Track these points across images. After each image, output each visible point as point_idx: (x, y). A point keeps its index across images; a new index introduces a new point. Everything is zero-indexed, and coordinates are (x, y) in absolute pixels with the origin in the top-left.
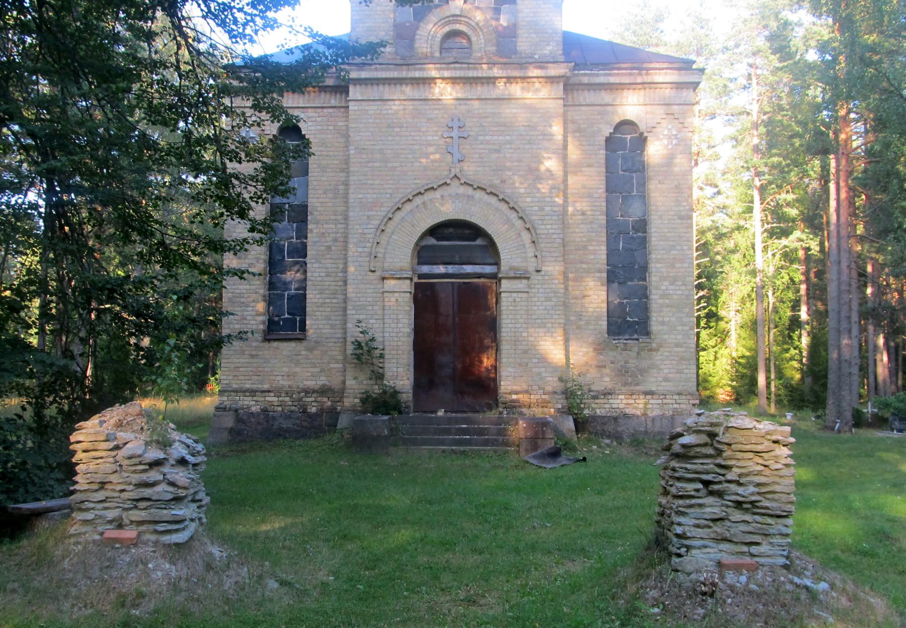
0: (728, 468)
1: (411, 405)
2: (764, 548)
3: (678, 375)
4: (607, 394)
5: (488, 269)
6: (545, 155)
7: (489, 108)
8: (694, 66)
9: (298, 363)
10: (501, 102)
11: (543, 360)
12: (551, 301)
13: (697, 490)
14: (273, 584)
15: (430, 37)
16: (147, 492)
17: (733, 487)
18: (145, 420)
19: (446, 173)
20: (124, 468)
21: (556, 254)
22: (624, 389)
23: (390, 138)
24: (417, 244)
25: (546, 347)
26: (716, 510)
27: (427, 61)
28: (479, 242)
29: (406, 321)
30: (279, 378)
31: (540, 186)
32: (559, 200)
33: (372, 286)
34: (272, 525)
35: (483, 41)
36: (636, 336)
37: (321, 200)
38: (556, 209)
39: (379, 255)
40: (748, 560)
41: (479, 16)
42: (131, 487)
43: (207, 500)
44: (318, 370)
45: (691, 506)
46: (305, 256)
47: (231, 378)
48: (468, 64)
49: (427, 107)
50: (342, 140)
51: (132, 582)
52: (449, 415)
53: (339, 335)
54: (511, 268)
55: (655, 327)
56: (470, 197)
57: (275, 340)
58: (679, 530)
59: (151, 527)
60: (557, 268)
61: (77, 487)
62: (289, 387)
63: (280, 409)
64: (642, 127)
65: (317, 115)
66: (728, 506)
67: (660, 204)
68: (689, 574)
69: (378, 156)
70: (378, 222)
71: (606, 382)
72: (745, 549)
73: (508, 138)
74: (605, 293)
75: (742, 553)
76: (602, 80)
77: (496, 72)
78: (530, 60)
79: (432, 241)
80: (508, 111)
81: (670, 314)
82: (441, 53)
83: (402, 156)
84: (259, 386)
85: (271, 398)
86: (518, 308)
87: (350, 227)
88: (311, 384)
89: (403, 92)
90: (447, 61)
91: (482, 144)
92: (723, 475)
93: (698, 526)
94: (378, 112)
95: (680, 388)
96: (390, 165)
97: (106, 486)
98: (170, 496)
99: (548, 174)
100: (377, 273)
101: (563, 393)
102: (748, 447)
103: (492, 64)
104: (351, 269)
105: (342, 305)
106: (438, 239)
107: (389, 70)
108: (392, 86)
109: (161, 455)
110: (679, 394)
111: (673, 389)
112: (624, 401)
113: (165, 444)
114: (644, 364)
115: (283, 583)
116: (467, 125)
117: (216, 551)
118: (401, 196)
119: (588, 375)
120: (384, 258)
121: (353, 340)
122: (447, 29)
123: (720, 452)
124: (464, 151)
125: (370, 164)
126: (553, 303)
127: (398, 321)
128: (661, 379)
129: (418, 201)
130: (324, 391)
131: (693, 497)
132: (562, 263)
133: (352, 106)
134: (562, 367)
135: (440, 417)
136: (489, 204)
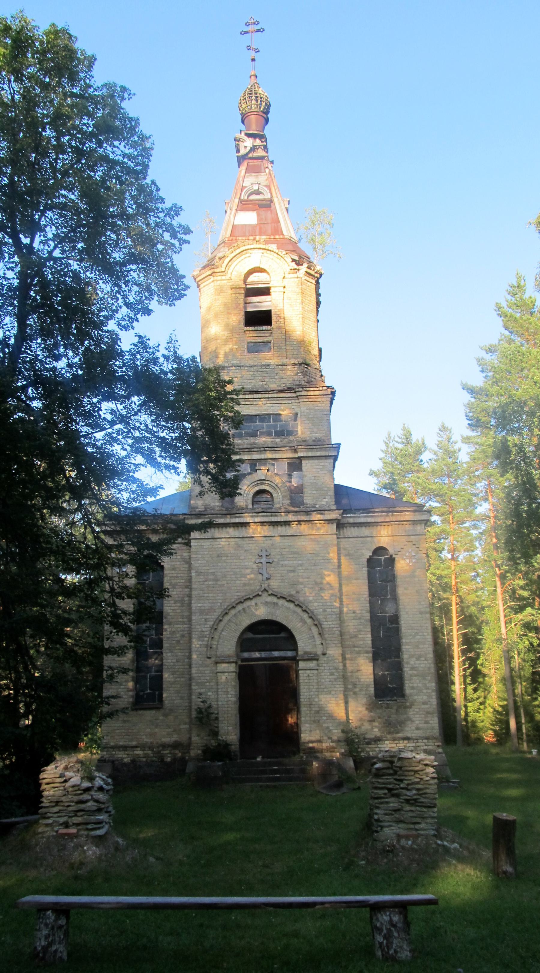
0: (401, 781)
1: (238, 754)
2: (423, 826)
3: (426, 725)
4: (377, 740)
5: (290, 654)
6: (326, 573)
7: (287, 542)
8: (425, 509)
9: (157, 726)
10: (294, 538)
11: (331, 717)
13: (385, 794)
14: (152, 859)
16: (82, 806)
17: (404, 791)
18: (80, 765)
19: (258, 588)
20: (70, 793)
21: (336, 642)
22: (389, 736)
23: (220, 564)
24: (240, 637)
25: (332, 708)
26: (395, 805)
27: (244, 511)
28: (283, 635)
29: (234, 693)
30: (144, 737)
31: (323, 595)
32: (337, 604)
33: (208, 669)
34: (148, 833)
35: (281, 497)
36: (395, 698)
38: (335, 610)
39: (214, 646)
40: (414, 832)
41: (277, 480)
42: (73, 804)
43: (113, 812)
44: (171, 730)
45: (382, 803)
46: (161, 647)
50: (187, 566)
51: (76, 856)
52: (266, 760)
53: (187, 704)
54: (306, 653)
55: (408, 691)
56: (275, 604)
57: (141, 709)
58: (376, 817)
59: (84, 827)
60: (337, 652)
61: (42, 805)
62: (152, 743)
63: (144, 760)
64: (391, 551)
66: (402, 802)
68: (382, 842)
69: (211, 577)
70: (212, 623)
71: (376, 732)
72: (412, 826)
73: (300, 562)
74: (372, 668)
75: (411, 829)
76: (362, 520)
77: (290, 517)
78: (313, 509)
79: (250, 635)
80: (301, 543)
81: (418, 681)
82: (253, 505)
84: (130, 743)
85: (139, 752)
87: (193, 627)
88: (166, 740)
89: (228, 533)
90: (257, 510)
91: (282, 566)
92: (399, 785)
93: (386, 814)
95: (427, 735)
96: (219, 583)
97: (59, 804)
98: (95, 808)
99: (328, 586)
100: (213, 659)
101: (345, 741)
102: (411, 768)
103: (288, 512)
104: (194, 656)
105: (188, 682)
106: (254, 633)
108: (220, 529)
109: (90, 785)
110: (427, 738)
111: (423, 735)
112: (389, 746)
113: (91, 779)
114: (402, 717)
115: (157, 859)
117: (120, 840)
118: (228, 604)
119: (363, 727)
120: (217, 648)
121: (196, 707)
122: (257, 489)
123: (395, 773)
124: (270, 572)
126: (335, 677)
127: (227, 693)
128: (414, 728)
129: (240, 607)
130: (176, 745)
131: (381, 798)
132: (341, 648)
133: (193, 543)
134: (343, 722)
135: (259, 761)
136: (288, 608)
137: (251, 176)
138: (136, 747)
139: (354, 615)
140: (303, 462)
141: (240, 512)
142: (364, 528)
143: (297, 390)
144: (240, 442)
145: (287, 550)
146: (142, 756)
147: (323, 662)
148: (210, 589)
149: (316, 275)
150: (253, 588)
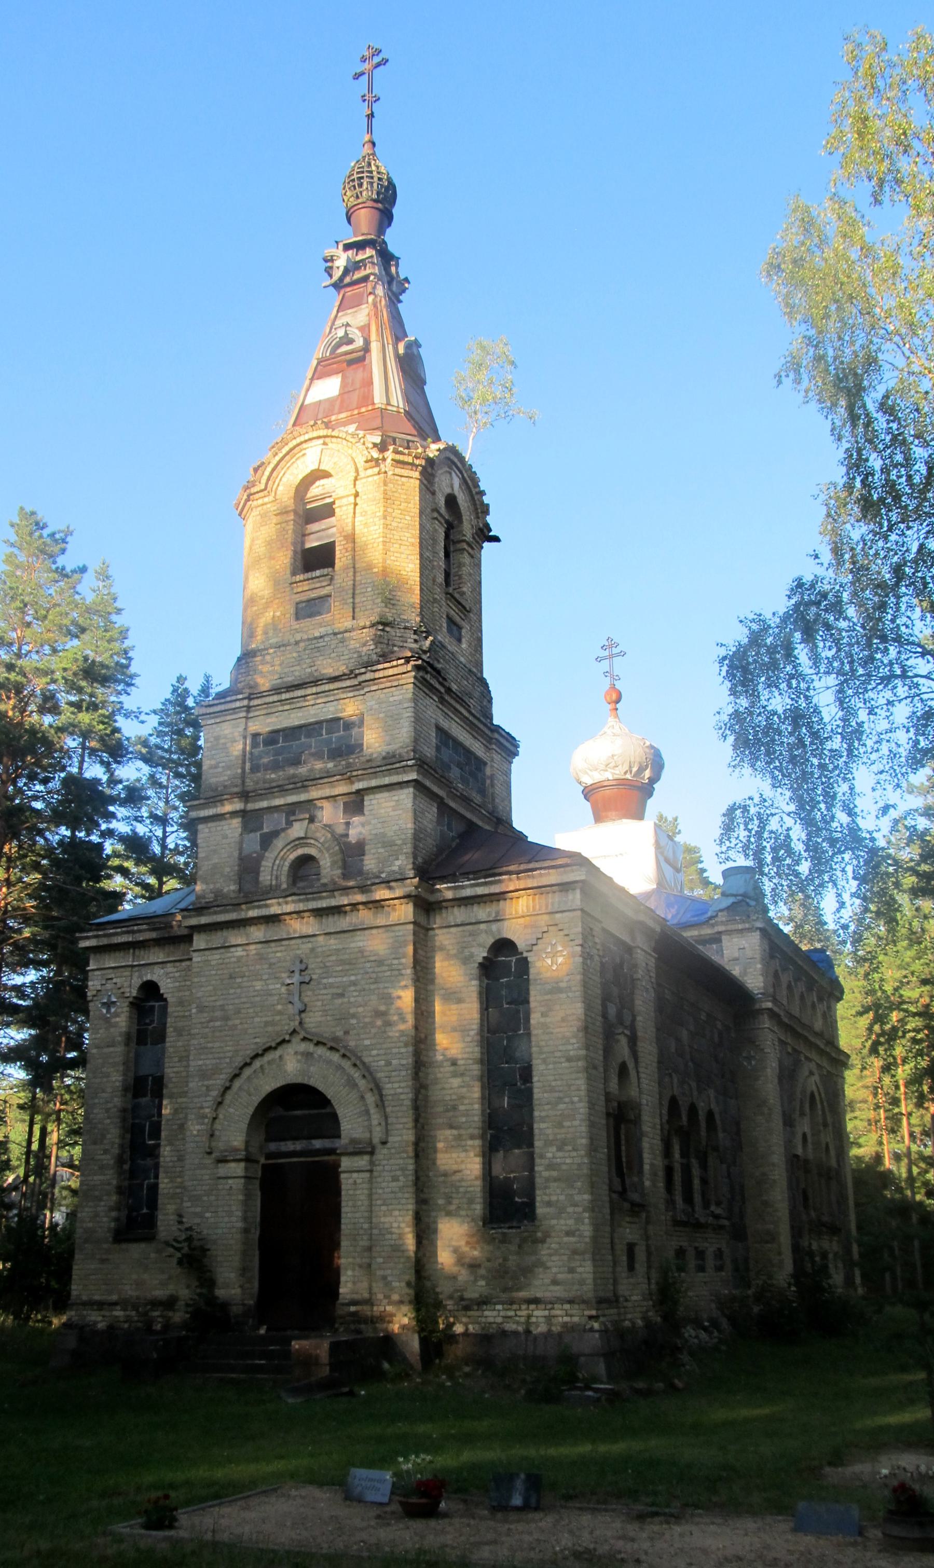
3: (570, 1276)
7: (333, 942)
12: (398, 1180)
15: (275, 868)
21: (404, 1120)
22: (504, 1296)
23: (232, 991)
27: (270, 896)
37: (175, 1070)
47: (81, 1287)
48: (306, 894)
49: (270, 950)
54: (353, 1141)
55: (540, 1210)
62: (138, 1298)
63: (126, 1326)
65: (175, 970)
67: (543, 1043)
69: (218, 1014)
73: (353, 978)
76: (480, 891)
78: (377, 881)
81: (558, 1191)
83: (243, 1011)
85: (118, 1313)
86: (358, 1192)
91: (325, 988)
94: (221, 961)
95: (572, 1294)
96: (230, 1023)
107: (227, 911)
110: (571, 1302)
112: (502, 1313)
116: (310, 967)
124: (306, 1000)
125: (211, 1024)
126: (401, 1184)
128: (547, 1281)
133: (196, 958)
137: (346, 314)
138: (115, 1304)
139: (452, 1068)
140: (366, 798)
141: (265, 897)
142: (475, 907)
143: (357, 671)
144: (273, 776)
145: (334, 958)
146: (122, 1319)
147: (381, 1157)
148: (218, 1034)
149: (417, 462)
150: (278, 1028)
